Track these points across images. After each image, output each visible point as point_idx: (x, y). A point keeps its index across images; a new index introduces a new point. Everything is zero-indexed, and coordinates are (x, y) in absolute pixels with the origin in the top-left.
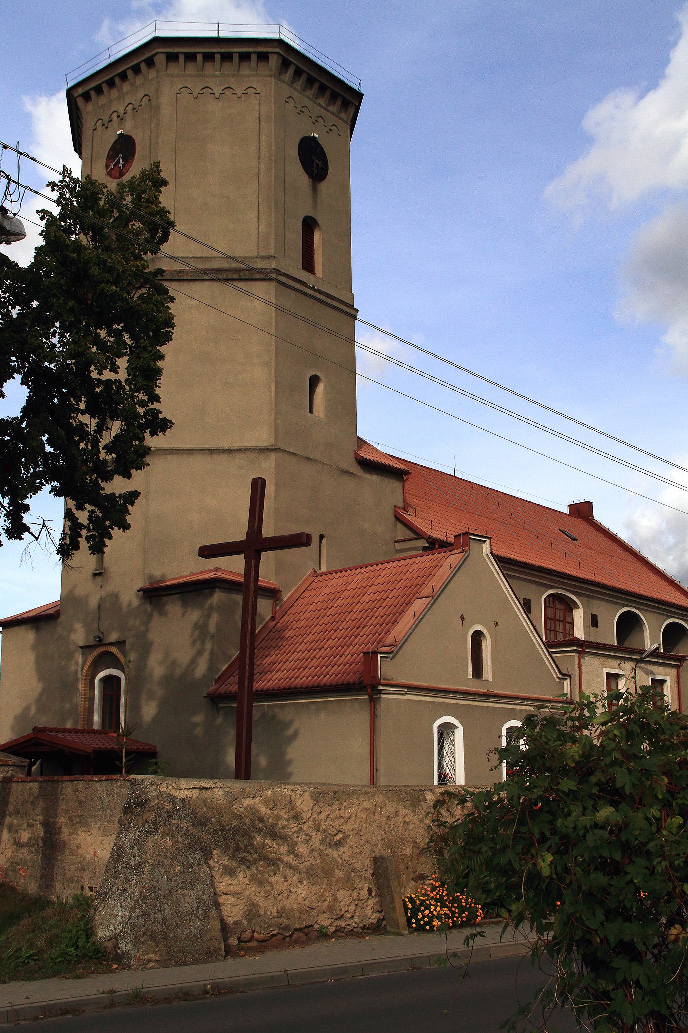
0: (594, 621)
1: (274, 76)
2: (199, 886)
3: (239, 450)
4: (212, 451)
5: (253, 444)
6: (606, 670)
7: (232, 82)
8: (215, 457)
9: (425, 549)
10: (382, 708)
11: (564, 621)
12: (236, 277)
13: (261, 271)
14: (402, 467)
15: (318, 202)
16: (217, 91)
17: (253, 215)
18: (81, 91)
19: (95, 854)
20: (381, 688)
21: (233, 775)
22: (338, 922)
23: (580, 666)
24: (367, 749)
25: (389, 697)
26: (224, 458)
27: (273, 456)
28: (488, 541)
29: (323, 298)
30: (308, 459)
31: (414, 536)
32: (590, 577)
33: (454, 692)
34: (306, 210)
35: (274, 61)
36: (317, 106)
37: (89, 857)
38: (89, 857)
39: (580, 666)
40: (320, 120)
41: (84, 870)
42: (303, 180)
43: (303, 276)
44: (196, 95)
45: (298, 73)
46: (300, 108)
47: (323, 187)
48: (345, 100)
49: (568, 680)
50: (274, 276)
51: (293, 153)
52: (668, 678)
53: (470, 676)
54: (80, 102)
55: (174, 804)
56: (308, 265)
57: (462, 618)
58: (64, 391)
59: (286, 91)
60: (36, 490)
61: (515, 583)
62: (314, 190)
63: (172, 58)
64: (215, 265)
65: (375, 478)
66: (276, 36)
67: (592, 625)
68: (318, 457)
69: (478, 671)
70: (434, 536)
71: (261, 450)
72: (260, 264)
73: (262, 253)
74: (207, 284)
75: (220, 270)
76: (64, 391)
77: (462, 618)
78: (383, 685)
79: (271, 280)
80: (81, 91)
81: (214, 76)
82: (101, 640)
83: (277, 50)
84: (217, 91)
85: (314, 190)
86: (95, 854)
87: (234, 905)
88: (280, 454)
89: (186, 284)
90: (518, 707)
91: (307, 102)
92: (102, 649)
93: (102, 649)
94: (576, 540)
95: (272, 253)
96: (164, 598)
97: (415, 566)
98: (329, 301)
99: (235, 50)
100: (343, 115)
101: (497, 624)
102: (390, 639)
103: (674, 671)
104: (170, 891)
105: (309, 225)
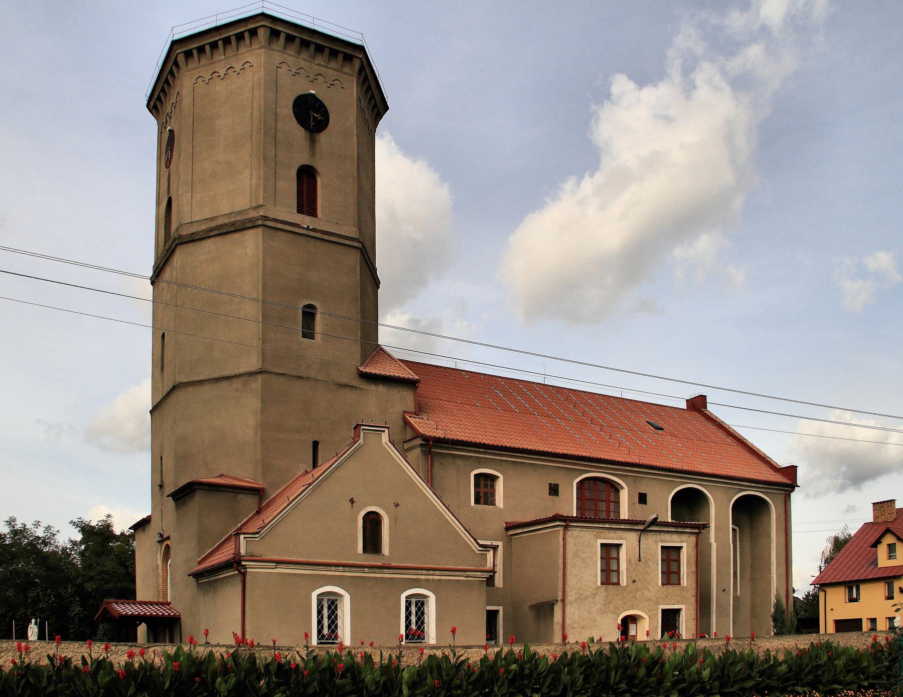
0: (643, 499)
1: (264, 47)
3: (236, 376)
4: (217, 380)
5: (247, 370)
6: (600, 541)
8: (219, 384)
11: (608, 502)
12: (233, 229)
13: (250, 220)
15: (317, 151)
16: (222, 72)
17: (248, 172)
20: (243, 563)
23: (564, 539)
25: (254, 570)
26: (225, 384)
27: (260, 378)
28: (387, 430)
29: (319, 235)
30: (300, 377)
33: (344, 566)
34: (304, 160)
35: (262, 34)
39: (564, 539)
40: (319, 77)
42: (299, 133)
43: (305, 221)
44: (207, 81)
45: (290, 39)
46: (294, 71)
47: (323, 138)
49: (492, 552)
50: (260, 222)
51: (286, 110)
57: (352, 501)
59: (278, 57)
61: (319, 464)
62: (313, 141)
63: (188, 54)
64: (220, 222)
65: (381, 389)
66: (259, 11)
67: (640, 502)
68: (313, 375)
70: (428, 434)
71: (251, 374)
72: (252, 214)
73: (254, 205)
74: (213, 239)
75: (222, 226)
77: (352, 501)
78: (245, 561)
79: (258, 226)
81: (221, 61)
83: (262, 23)
84: (222, 72)
88: (267, 376)
89: (198, 243)
90: (431, 577)
91: (303, 63)
94: (662, 429)
95: (261, 202)
98: (326, 237)
99: (231, 33)
100: (347, 69)
103: (693, 539)
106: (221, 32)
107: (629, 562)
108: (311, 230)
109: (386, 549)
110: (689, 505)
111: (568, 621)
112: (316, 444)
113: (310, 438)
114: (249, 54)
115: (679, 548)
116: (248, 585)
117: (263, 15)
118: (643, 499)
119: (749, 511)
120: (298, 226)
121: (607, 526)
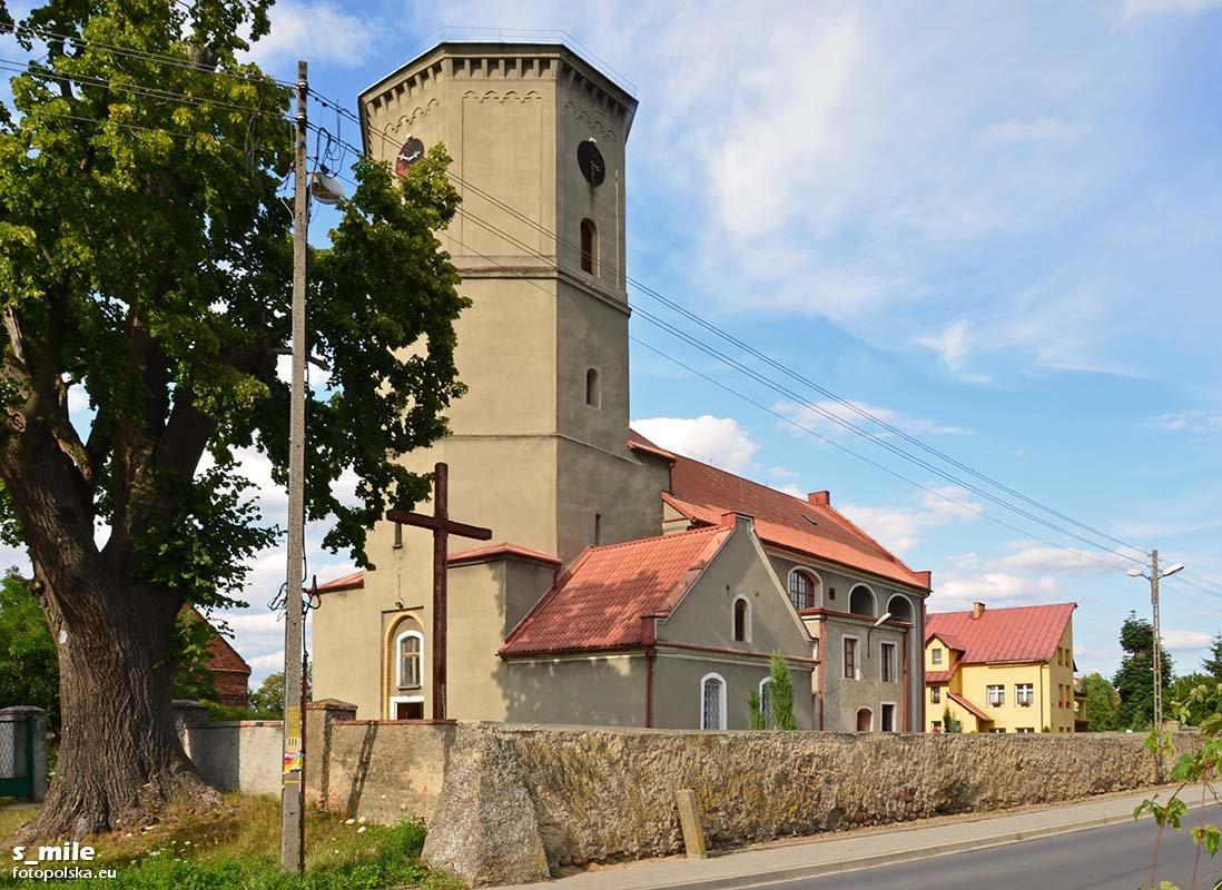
0: (832, 594)
2: (525, 819)
6: (844, 636)
7: (515, 86)
9: (689, 528)
10: (657, 666)
14: (670, 455)
18: (371, 97)
19: (426, 789)
20: (657, 648)
21: (645, 724)
22: (645, 849)
24: (643, 701)
25: (663, 654)
31: (682, 517)
32: (831, 557)
36: (597, 113)
37: (420, 792)
38: (420, 792)
41: (416, 802)
42: (582, 182)
43: (583, 275)
45: (578, 78)
47: (601, 190)
48: (614, 103)
51: (574, 157)
52: (896, 644)
53: (734, 638)
54: (370, 108)
55: (500, 745)
56: (587, 265)
57: (728, 588)
58: (169, 370)
60: (337, 474)
62: (592, 193)
69: (740, 635)
71: (544, 437)
76: (169, 370)
77: (728, 588)
80: (371, 97)
82: (401, 606)
84: (502, 95)
85: (592, 193)
86: (426, 789)
87: (555, 834)
92: (401, 614)
93: (401, 614)
96: (542, 568)
97: (685, 542)
101: (757, 595)
102: (665, 606)
104: (499, 824)
105: (587, 228)
106: (507, 50)
107: (862, 658)
108: (593, 290)
109: (748, 638)
110: (861, 600)
111: (824, 713)
112: (598, 516)
113: (593, 509)
114: (537, 84)
115: (893, 646)
116: (655, 679)
117: (562, 48)
118: (832, 594)
119: (898, 608)
120: (582, 283)
121: (860, 623)
